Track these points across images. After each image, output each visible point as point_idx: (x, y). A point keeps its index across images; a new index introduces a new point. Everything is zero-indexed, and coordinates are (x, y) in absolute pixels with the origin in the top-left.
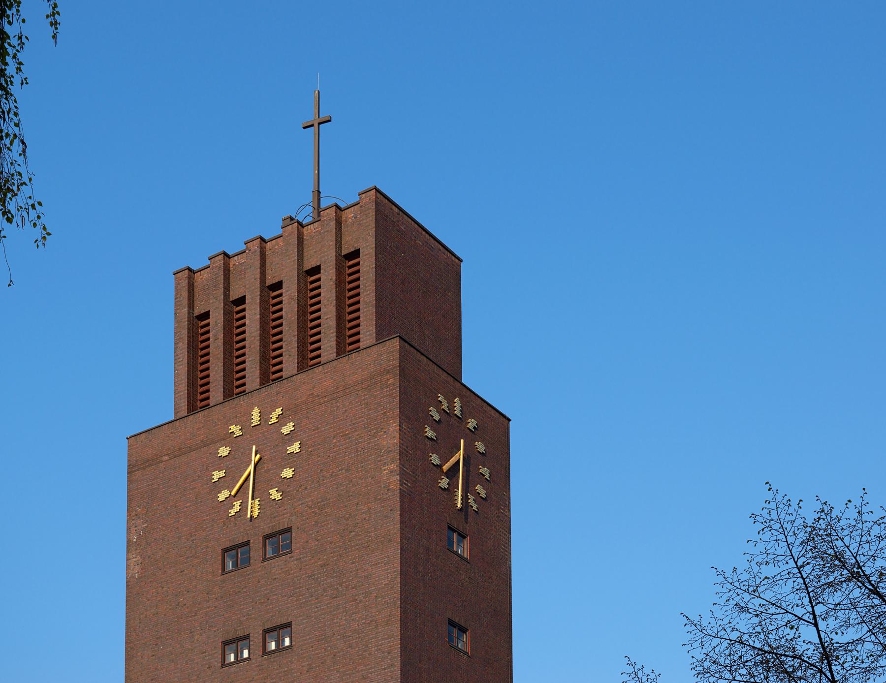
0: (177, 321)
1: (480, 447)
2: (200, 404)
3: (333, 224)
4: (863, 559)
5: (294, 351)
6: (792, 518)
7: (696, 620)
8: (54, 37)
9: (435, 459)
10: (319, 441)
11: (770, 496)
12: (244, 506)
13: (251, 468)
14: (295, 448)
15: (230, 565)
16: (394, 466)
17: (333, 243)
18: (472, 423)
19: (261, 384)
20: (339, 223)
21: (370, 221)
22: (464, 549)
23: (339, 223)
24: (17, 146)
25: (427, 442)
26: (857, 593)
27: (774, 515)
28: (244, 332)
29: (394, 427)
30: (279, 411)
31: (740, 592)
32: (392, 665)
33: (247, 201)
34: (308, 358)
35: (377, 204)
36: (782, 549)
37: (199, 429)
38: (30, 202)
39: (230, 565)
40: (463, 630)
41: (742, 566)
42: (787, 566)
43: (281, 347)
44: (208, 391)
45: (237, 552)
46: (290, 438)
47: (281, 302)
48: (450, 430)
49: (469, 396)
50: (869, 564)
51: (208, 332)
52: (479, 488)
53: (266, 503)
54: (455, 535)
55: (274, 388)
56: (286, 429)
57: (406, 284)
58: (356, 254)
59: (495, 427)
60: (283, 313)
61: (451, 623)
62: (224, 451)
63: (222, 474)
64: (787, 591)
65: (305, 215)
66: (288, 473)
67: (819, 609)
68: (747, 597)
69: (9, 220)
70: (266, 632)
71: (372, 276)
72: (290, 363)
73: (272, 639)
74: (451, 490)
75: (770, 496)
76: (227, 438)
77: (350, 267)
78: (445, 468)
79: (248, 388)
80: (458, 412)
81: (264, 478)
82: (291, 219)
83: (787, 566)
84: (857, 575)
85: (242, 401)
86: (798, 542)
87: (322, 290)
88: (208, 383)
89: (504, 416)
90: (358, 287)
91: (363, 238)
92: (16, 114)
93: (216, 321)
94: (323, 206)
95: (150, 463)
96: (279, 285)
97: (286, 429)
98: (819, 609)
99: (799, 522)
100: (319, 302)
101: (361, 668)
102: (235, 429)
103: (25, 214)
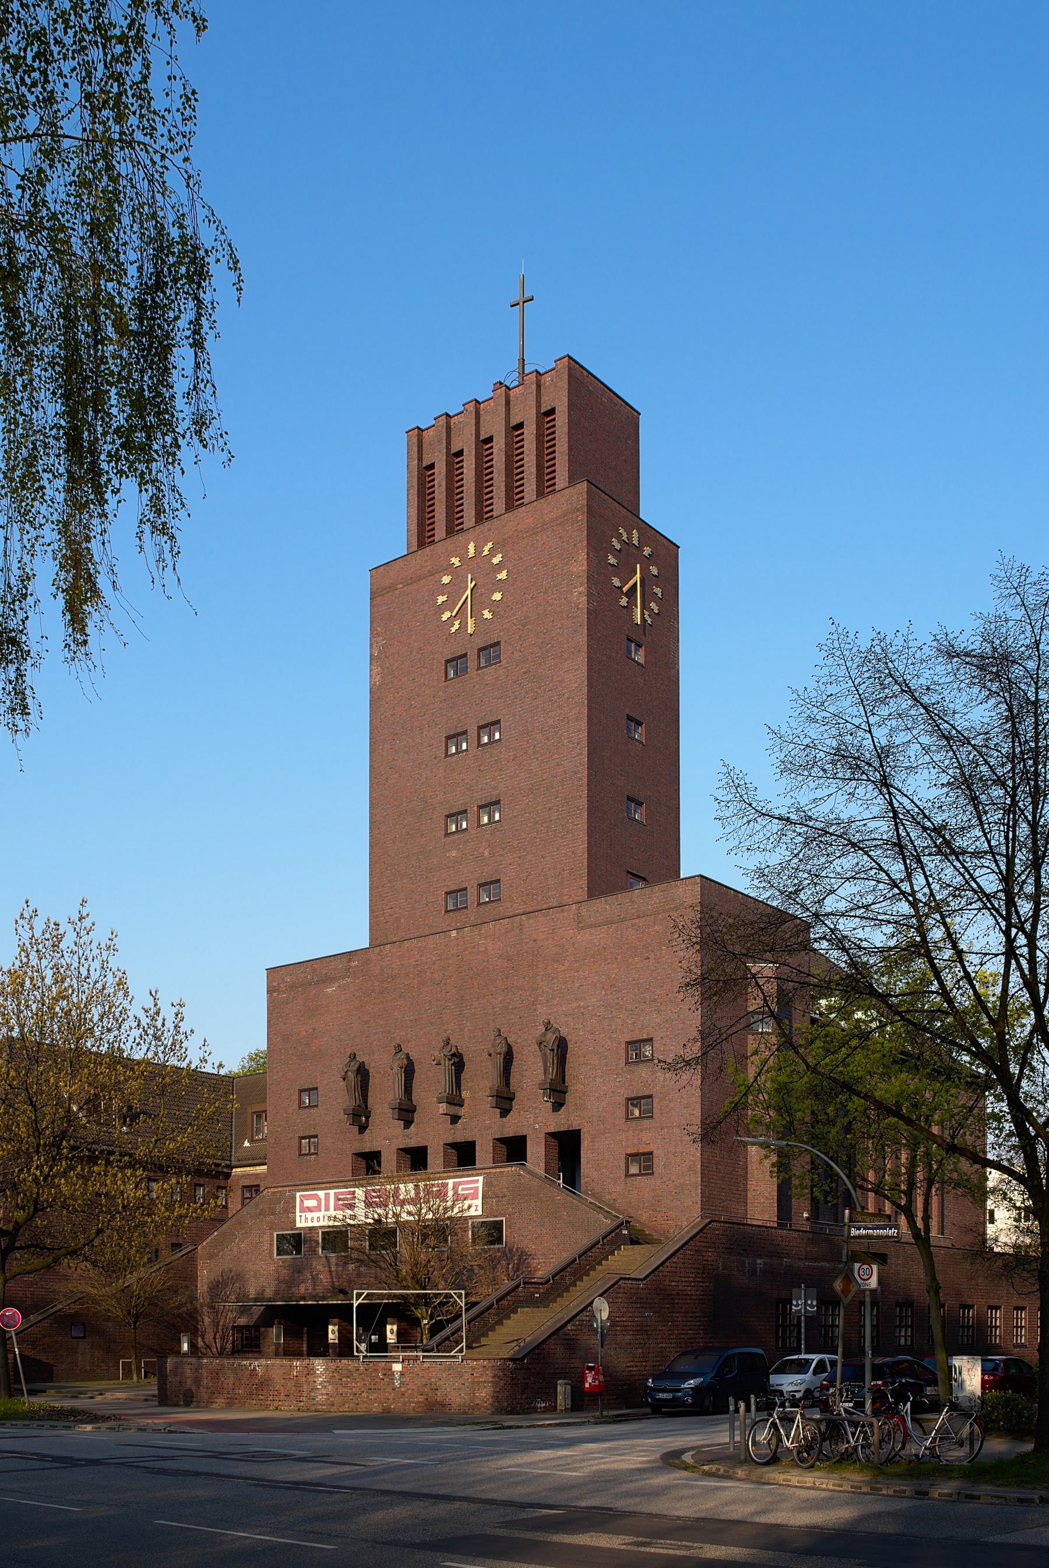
1: (654, 570)
2: (428, 541)
3: (534, 386)
4: (909, 677)
5: (503, 494)
6: (851, 647)
8: (239, 300)
9: (616, 582)
10: (523, 567)
11: (833, 629)
12: (464, 625)
13: (469, 592)
14: (503, 575)
15: (452, 674)
16: (582, 589)
17: (534, 403)
18: (647, 551)
19: (506, 509)
20: (539, 386)
21: (564, 384)
22: (640, 657)
23: (539, 386)
24: (209, 389)
25: (610, 568)
27: (836, 645)
28: (462, 479)
29: (583, 556)
30: (490, 545)
31: (810, 706)
32: (581, 754)
33: (462, 373)
34: (513, 501)
35: (569, 369)
37: (426, 561)
38: (219, 432)
39: (452, 674)
40: (640, 724)
41: (812, 685)
42: (847, 685)
43: (492, 491)
44: (433, 529)
45: (457, 661)
46: (499, 567)
47: (492, 454)
48: (629, 555)
50: (914, 681)
51: (433, 480)
52: (653, 605)
53: (479, 620)
54: (633, 645)
55: (487, 525)
56: (496, 560)
57: (592, 435)
58: (552, 411)
59: (666, 553)
60: (494, 462)
61: (630, 718)
62: (446, 579)
63: (445, 598)
65: (512, 381)
66: (497, 596)
69: (205, 446)
70: (480, 728)
71: (566, 429)
72: (499, 504)
73: (485, 733)
75: (833, 629)
76: (449, 569)
77: (548, 422)
78: (625, 589)
79: (465, 526)
80: (636, 542)
81: (479, 600)
82: (501, 383)
83: (847, 685)
84: (907, 690)
85: (460, 538)
86: (855, 666)
87: (525, 443)
88: (433, 523)
89: (674, 544)
90: (554, 439)
91: (559, 399)
92: (209, 364)
93: (440, 470)
94: (526, 372)
95: (388, 588)
96: (490, 440)
97: (496, 560)
98: (872, 720)
99: (855, 650)
100: (522, 453)
101: (556, 756)
102: (455, 561)
103: (215, 442)
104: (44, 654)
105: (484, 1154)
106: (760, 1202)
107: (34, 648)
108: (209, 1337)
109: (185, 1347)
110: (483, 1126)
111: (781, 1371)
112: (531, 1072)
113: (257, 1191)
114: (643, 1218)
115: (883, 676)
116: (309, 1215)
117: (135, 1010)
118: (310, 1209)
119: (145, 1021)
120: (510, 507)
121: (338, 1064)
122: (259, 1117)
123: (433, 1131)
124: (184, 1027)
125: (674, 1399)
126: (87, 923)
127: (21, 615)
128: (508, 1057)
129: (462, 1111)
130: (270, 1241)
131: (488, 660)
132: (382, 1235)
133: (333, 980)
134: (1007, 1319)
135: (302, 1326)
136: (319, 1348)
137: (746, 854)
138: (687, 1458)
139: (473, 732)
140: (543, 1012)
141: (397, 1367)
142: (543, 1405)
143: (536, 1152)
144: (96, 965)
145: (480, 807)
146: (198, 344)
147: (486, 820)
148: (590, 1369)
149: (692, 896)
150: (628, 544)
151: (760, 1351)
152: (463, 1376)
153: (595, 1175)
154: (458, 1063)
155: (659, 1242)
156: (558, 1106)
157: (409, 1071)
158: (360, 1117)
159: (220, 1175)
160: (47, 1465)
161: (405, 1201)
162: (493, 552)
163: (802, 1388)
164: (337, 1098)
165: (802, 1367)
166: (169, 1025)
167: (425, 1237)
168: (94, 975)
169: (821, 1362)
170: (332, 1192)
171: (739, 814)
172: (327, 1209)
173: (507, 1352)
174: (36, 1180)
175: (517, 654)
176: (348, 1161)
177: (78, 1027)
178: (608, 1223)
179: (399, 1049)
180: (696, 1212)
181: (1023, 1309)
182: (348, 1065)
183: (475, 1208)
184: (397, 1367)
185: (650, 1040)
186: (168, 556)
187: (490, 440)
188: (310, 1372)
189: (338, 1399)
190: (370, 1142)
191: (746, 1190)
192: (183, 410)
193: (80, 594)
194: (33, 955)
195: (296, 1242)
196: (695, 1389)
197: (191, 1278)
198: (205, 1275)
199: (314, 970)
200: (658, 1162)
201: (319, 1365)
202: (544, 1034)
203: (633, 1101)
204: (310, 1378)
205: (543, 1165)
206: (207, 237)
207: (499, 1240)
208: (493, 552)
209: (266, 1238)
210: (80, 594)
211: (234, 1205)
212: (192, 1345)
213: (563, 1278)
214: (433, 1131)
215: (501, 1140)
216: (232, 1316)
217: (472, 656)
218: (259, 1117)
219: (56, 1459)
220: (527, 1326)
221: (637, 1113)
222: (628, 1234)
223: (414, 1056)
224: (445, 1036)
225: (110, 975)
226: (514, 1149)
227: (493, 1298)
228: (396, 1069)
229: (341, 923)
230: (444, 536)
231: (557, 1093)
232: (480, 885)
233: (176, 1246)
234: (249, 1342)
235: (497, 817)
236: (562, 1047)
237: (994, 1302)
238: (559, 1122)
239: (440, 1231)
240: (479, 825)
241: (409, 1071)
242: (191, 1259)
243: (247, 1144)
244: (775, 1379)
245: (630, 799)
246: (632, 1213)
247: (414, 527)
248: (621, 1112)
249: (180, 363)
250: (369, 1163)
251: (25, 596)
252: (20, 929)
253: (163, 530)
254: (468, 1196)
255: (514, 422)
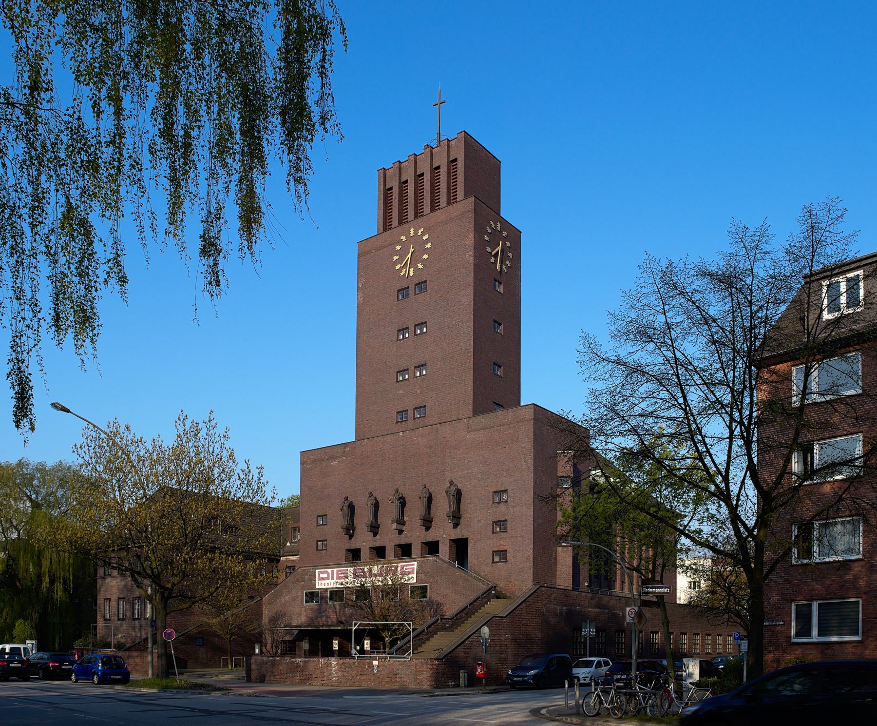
0: (379, 191)
1: (508, 244)
7: (613, 312)
10: (439, 242)
11: (647, 257)
13: (410, 255)
14: (429, 246)
17: (446, 156)
18: (505, 234)
23: (448, 147)
26: (682, 300)
29: (471, 236)
33: (407, 139)
36: (651, 281)
40: (500, 324)
41: (634, 288)
45: (403, 291)
46: (427, 241)
48: (495, 237)
49: (504, 222)
53: (416, 270)
55: (420, 219)
56: (425, 238)
57: (477, 173)
58: (456, 160)
59: (515, 235)
61: (495, 321)
62: (398, 248)
64: (653, 299)
65: (434, 144)
66: (426, 257)
67: (667, 307)
68: (635, 302)
70: (416, 326)
72: (427, 209)
74: (495, 263)
75: (647, 257)
76: (400, 242)
79: (408, 220)
85: (406, 226)
95: (368, 254)
96: (422, 175)
97: (425, 238)
98: (667, 307)
99: (659, 268)
102: (404, 238)
104: (230, 252)
105: (416, 550)
106: (564, 576)
107: (224, 248)
108: (269, 646)
109: (257, 651)
110: (415, 535)
111: (577, 666)
112: (442, 507)
113: (294, 569)
114: (502, 585)
115: (670, 284)
116: (323, 582)
117: (238, 470)
118: (323, 579)
119: (242, 476)
120: (433, 209)
121: (338, 503)
122: (295, 530)
123: (389, 538)
124: (263, 480)
125: (523, 681)
126: (213, 423)
127: (217, 229)
128: (430, 499)
129: (404, 528)
130: (302, 595)
131: (420, 290)
132: (363, 593)
133: (336, 458)
134: (690, 640)
135: (318, 641)
136: (328, 652)
137: (594, 382)
138: (543, 711)
139: (412, 328)
140: (448, 476)
141: (376, 663)
143: (444, 549)
144: (218, 445)
145: (415, 367)
146: (323, 74)
147: (418, 374)
148: (480, 664)
149: (530, 414)
150: (495, 230)
151: (568, 656)
152: (411, 669)
153: (476, 562)
154: (403, 502)
155: (510, 597)
156: (456, 525)
157: (376, 506)
158: (350, 530)
159: (274, 560)
160: (197, 714)
161: (375, 575)
162: (423, 234)
163: (589, 675)
164: (338, 520)
165: (588, 664)
166: (255, 478)
167: (388, 594)
168: (217, 451)
169: (599, 662)
170: (335, 570)
171: (591, 360)
172: (333, 579)
173: (435, 655)
174: (185, 561)
175: (436, 287)
176: (342, 554)
177: (208, 480)
178: (484, 588)
179: (371, 495)
180: (530, 583)
181: (698, 634)
182: (344, 503)
183: (413, 579)
184: (376, 663)
185: (506, 491)
186: (303, 195)
187: (422, 175)
188: (329, 665)
189: (344, 680)
190: (355, 544)
191: (556, 571)
192: (315, 112)
193: (251, 216)
194: (185, 439)
195: (312, 596)
196: (534, 676)
197: (259, 615)
198: (267, 613)
199: (326, 453)
200: (510, 555)
201: (334, 661)
202: (449, 487)
203: (496, 523)
204: (329, 668)
205: (447, 556)
206: (329, 14)
207: (425, 597)
208: (423, 234)
209: (300, 594)
210: (251, 216)
211: (282, 576)
212: (261, 651)
213: (461, 616)
214: (389, 538)
215: (425, 543)
216: (282, 634)
217: (412, 288)
218: (295, 530)
219: (200, 711)
220: (443, 642)
221: (498, 530)
222: (493, 593)
223: (379, 498)
224: (395, 488)
225: (225, 451)
226: (432, 548)
227: (425, 626)
228: (369, 505)
229: (341, 429)
231: (456, 518)
232: (415, 409)
233: (251, 598)
234: (290, 648)
235: (424, 372)
236: (459, 494)
237: (683, 631)
238: (457, 534)
239: (393, 591)
240: (415, 377)
241: (376, 506)
242: (259, 605)
243: (288, 544)
244: (575, 671)
245: (495, 364)
246: (496, 582)
247: (381, 220)
248: (490, 528)
249: (311, 86)
250: (354, 555)
251: (219, 218)
252: (178, 426)
253: (298, 180)
254: (409, 572)
255: (435, 166)
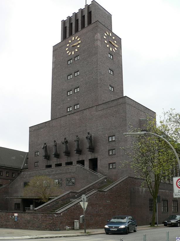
30: (77, 37)
63: (68, 49)
97: (78, 40)
139: (74, 73)
142: (69, 228)
143: (87, 163)
226: (82, 162)
230: (74, 33)
